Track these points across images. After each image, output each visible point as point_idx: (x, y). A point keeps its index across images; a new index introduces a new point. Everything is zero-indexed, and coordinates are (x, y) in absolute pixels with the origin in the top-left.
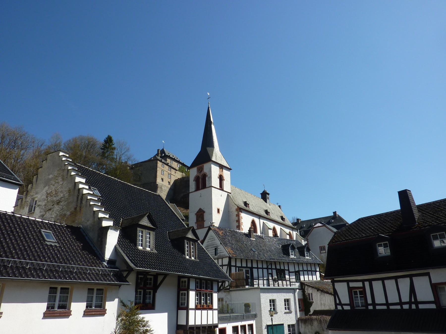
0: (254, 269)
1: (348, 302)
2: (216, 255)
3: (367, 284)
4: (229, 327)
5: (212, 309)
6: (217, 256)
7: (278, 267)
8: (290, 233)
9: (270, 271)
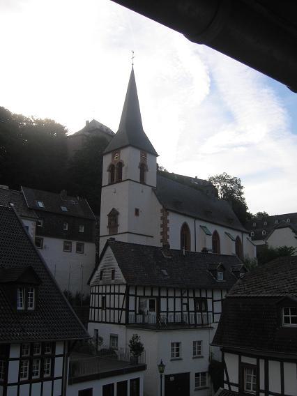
0: (162, 299)
1: (237, 382)
2: (113, 279)
3: (262, 363)
4: (97, 387)
5: (52, 379)
6: (113, 281)
7: (197, 295)
8: (238, 237)
9: (185, 301)
